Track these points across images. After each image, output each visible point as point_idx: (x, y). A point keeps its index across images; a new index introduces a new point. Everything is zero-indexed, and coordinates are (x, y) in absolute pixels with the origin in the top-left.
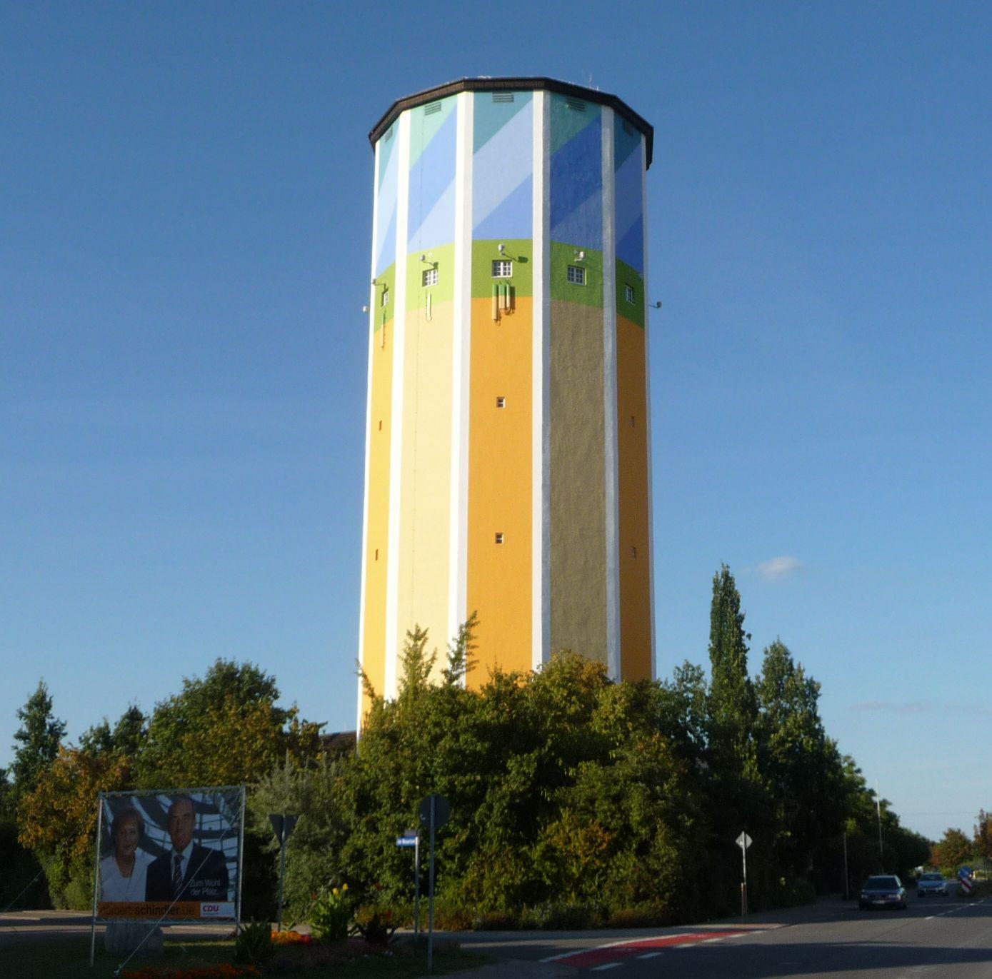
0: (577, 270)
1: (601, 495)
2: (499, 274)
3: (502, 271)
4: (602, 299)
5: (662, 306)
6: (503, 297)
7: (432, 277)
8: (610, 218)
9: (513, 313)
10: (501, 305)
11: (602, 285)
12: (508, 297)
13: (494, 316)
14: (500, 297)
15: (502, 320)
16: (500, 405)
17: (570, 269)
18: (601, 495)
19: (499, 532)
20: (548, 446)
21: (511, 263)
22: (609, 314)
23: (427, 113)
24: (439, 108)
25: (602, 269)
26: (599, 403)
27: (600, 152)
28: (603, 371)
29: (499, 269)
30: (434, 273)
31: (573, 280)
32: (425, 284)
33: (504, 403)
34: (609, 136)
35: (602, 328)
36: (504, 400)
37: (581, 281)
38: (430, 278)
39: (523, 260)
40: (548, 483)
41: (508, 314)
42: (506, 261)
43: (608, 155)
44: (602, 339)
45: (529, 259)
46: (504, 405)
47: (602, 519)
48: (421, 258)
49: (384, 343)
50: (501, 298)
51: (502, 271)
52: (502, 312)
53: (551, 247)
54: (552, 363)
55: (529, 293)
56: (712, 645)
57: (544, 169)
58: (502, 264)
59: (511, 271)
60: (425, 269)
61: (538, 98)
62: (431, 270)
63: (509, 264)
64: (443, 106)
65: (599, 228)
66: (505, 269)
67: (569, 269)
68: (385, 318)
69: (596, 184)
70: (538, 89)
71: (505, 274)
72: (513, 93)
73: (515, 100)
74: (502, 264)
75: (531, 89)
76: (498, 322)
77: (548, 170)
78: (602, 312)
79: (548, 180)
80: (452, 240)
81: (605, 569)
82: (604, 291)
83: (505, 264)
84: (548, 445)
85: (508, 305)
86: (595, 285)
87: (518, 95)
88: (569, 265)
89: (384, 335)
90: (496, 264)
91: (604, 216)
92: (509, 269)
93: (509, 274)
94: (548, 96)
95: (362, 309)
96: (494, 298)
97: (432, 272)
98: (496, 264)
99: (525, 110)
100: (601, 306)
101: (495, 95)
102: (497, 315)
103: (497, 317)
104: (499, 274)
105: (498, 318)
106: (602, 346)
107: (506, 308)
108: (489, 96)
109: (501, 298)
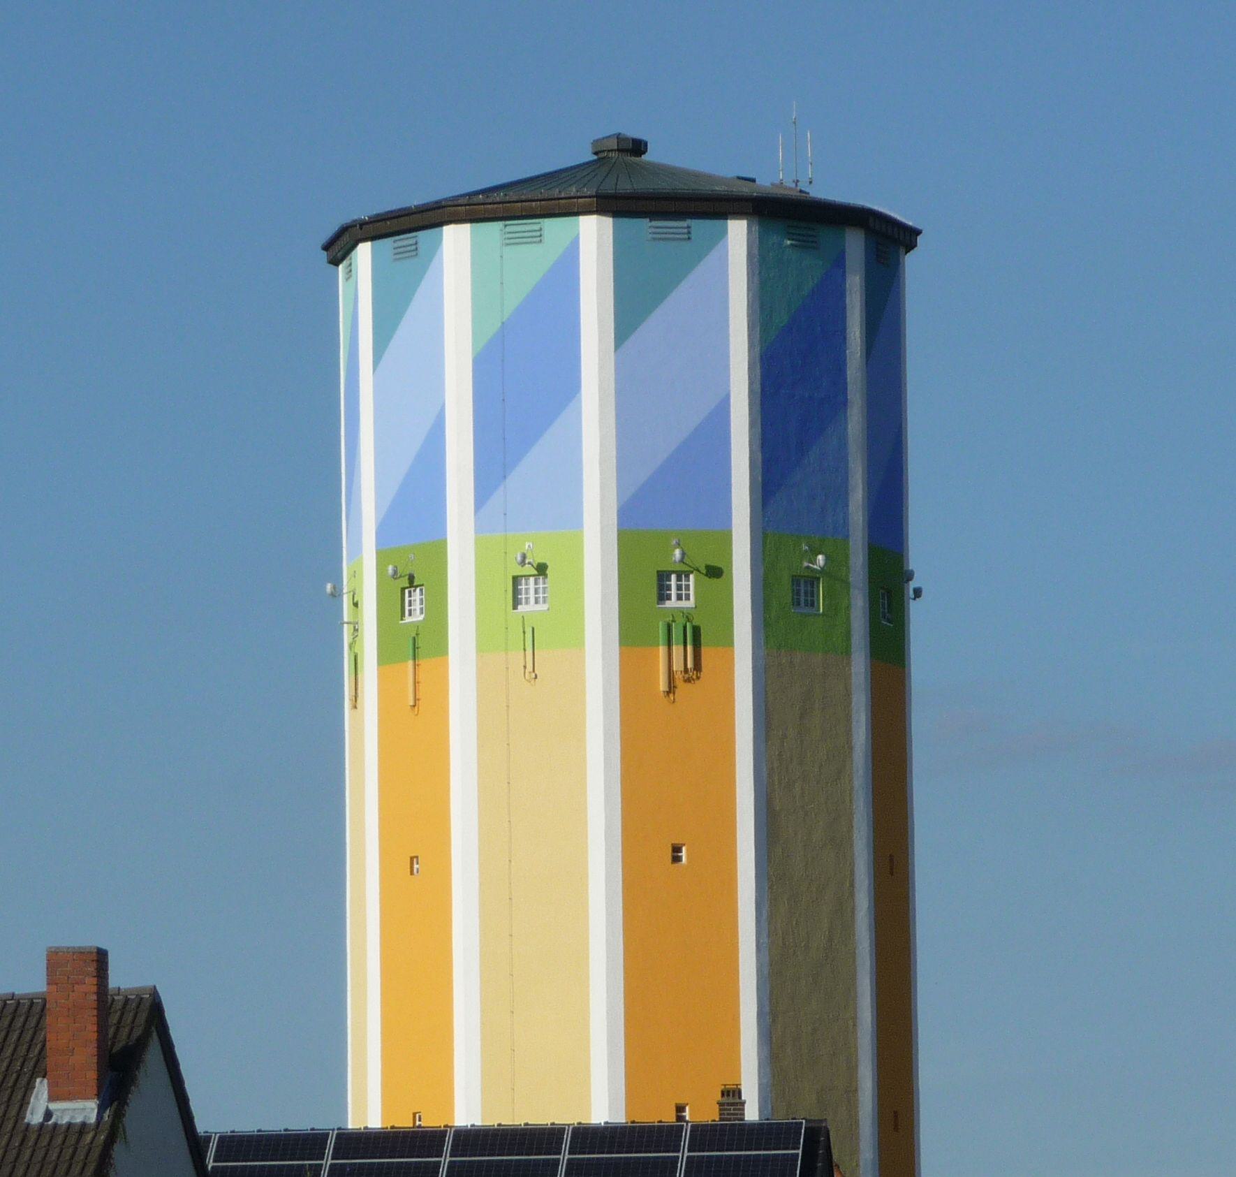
0: (805, 582)
1: (850, 1022)
2: (669, 598)
3: (673, 592)
4: (848, 635)
5: (924, 593)
6: (682, 647)
7: (532, 591)
8: (860, 469)
9: (698, 678)
10: (677, 666)
11: (848, 607)
12: (690, 648)
13: (662, 686)
14: (674, 647)
15: (677, 691)
16: (676, 859)
17: (796, 580)
18: (850, 1022)
19: (681, 1101)
20: (766, 940)
21: (692, 577)
22: (859, 666)
23: (511, 241)
24: (539, 238)
25: (847, 575)
26: (841, 845)
27: (844, 330)
28: (851, 780)
29: (669, 588)
30: (536, 583)
31: (799, 604)
32: (516, 603)
33: (684, 854)
34: (858, 293)
35: (848, 694)
36: (684, 849)
37: (812, 605)
38: (527, 590)
39: (715, 572)
40: (767, 1009)
41: (688, 680)
42: (683, 572)
43: (858, 334)
44: (848, 718)
45: (725, 570)
46: (684, 859)
47: (852, 1068)
48: (519, 559)
49: (416, 700)
50: (677, 650)
51: (673, 592)
52: (679, 677)
53: (764, 543)
54: (770, 776)
55: (727, 639)
56: (137, 1073)
57: (751, 384)
58: (673, 577)
59: (692, 592)
60: (515, 574)
61: (738, 231)
62: (530, 576)
63: (687, 577)
64: (546, 233)
65: (841, 494)
66: (679, 588)
67: (793, 581)
68: (415, 648)
69: (838, 402)
70: (738, 214)
71: (679, 598)
72: (688, 222)
73: (693, 236)
74: (673, 577)
75: (724, 215)
76: (671, 695)
77: (758, 387)
78: (849, 664)
79: (758, 408)
80: (578, 524)
81: (858, 1161)
82: (852, 617)
83: (679, 579)
84: (765, 940)
85: (690, 665)
86: (837, 608)
87: (699, 227)
88: (793, 576)
89: (415, 683)
90: (663, 577)
91: (851, 465)
92: (688, 587)
93: (688, 598)
94: (756, 228)
95: (325, 588)
96: (662, 650)
97: (532, 580)
98: (663, 577)
99: (711, 259)
100: (847, 653)
101: (655, 223)
102: (670, 683)
103: (670, 687)
104: (669, 598)
105: (671, 688)
106: (848, 732)
107: (686, 670)
108: (643, 227)
109: (677, 650)
